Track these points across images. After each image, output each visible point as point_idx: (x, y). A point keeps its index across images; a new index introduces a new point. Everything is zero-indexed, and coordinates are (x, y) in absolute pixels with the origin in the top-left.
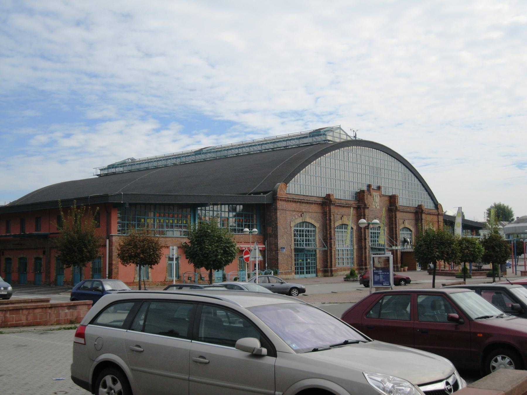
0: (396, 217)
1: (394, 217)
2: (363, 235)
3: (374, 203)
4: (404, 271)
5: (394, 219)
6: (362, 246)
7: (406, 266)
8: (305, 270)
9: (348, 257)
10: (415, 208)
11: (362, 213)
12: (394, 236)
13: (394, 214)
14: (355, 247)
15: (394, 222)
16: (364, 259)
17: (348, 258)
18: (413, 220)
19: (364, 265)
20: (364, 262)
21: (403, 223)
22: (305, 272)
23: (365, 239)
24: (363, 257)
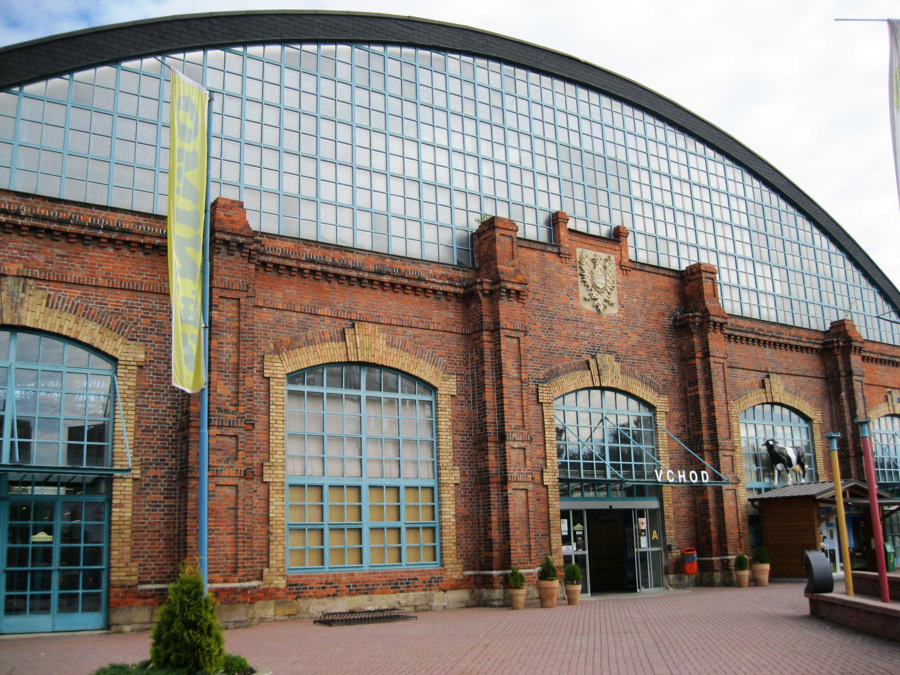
0: (706, 355)
1: (698, 355)
2: (491, 417)
3: (583, 292)
4: (755, 582)
5: (698, 362)
6: (486, 470)
7: (763, 562)
8: (55, 592)
9: (397, 524)
10: (822, 337)
11: (487, 319)
12: (705, 432)
13: (696, 340)
14: (452, 476)
15: (700, 375)
16: (495, 535)
17: (399, 529)
18: (819, 381)
19: (495, 563)
20: (496, 546)
21: (763, 386)
22: (54, 601)
23: (502, 437)
24: (495, 525)
